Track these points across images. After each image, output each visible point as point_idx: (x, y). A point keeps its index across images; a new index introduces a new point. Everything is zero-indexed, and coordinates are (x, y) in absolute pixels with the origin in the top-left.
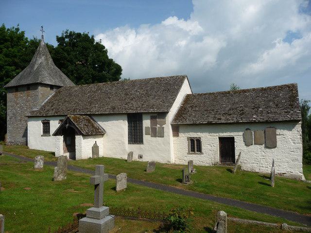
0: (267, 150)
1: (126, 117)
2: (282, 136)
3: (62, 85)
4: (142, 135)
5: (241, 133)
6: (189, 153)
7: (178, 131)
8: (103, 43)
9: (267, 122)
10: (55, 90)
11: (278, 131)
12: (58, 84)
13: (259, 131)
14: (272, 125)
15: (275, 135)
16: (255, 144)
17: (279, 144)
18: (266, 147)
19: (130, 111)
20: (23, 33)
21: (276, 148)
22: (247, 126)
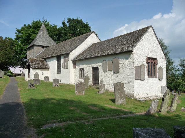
0: (115, 75)
1: (56, 58)
2: (123, 64)
3: (49, 46)
4: (61, 68)
5: (101, 64)
6: (80, 79)
7: (76, 65)
8: (168, 15)
9: (112, 55)
10: (44, 48)
11: (121, 61)
12: (47, 45)
13: (109, 61)
14: (117, 56)
15: (118, 64)
16: (108, 71)
17: (120, 70)
18: (114, 73)
19: (57, 55)
20: (49, 23)
21: (119, 74)
22: (104, 58)
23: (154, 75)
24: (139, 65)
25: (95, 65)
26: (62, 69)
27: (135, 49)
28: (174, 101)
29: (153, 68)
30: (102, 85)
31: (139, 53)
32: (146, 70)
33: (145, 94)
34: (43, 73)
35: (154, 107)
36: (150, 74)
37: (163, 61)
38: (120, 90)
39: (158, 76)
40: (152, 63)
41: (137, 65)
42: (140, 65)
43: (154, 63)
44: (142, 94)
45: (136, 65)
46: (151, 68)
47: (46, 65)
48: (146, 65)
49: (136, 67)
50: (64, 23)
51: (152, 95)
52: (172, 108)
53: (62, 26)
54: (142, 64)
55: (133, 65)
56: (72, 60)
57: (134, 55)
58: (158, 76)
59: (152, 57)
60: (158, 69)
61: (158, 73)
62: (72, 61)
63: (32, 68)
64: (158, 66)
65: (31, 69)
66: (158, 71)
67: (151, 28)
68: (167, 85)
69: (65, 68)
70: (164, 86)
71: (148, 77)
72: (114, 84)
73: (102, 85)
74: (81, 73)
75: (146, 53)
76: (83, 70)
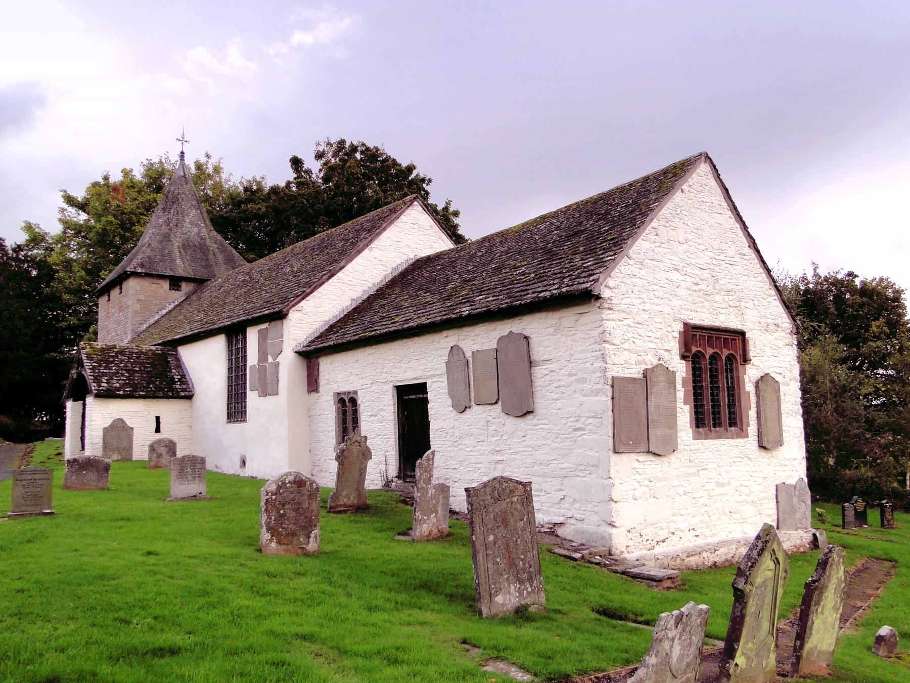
4: (245, 393)
23: (733, 423)
24: (635, 372)
25: (408, 377)
26: (253, 399)
27: (611, 282)
28: (815, 598)
29: (723, 383)
30: (431, 491)
31: (635, 302)
32: (680, 395)
33: (679, 534)
34: (158, 418)
35: (676, 651)
36: (709, 419)
37: (781, 344)
38: (505, 523)
39: (752, 429)
40: (714, 357)
41: (627, 374)
42: (646, 371)
43: (731, 358)
44: (663, 534)
45: (616, 371)
46: (715, 389)
47: (177, 378)
48: (681, 369)
49: (615, 383)
50: (296, 163)
51: (723, 537)
52: (808, 646)
53: (291, 175)
54: (655, 362)
55: (605, 371)
56: (300, 349)
57: (606, 314)
58: (752, 429)
59: (717, 324)
60: (749, 387)
61: (752, 414)
62: (299, 353)
63: (98, 396)
64: (750, 375)
65: (90, 400)
66: (753, 398)
67: (703, 168)
68: (808, 476)
69: (264, 393)
70: (792, 481)
71: (697, 437)
72: (467, 490)
73: (431, 491)
74: (344, 413)
75: (676, 303)
76: (353, 401)
